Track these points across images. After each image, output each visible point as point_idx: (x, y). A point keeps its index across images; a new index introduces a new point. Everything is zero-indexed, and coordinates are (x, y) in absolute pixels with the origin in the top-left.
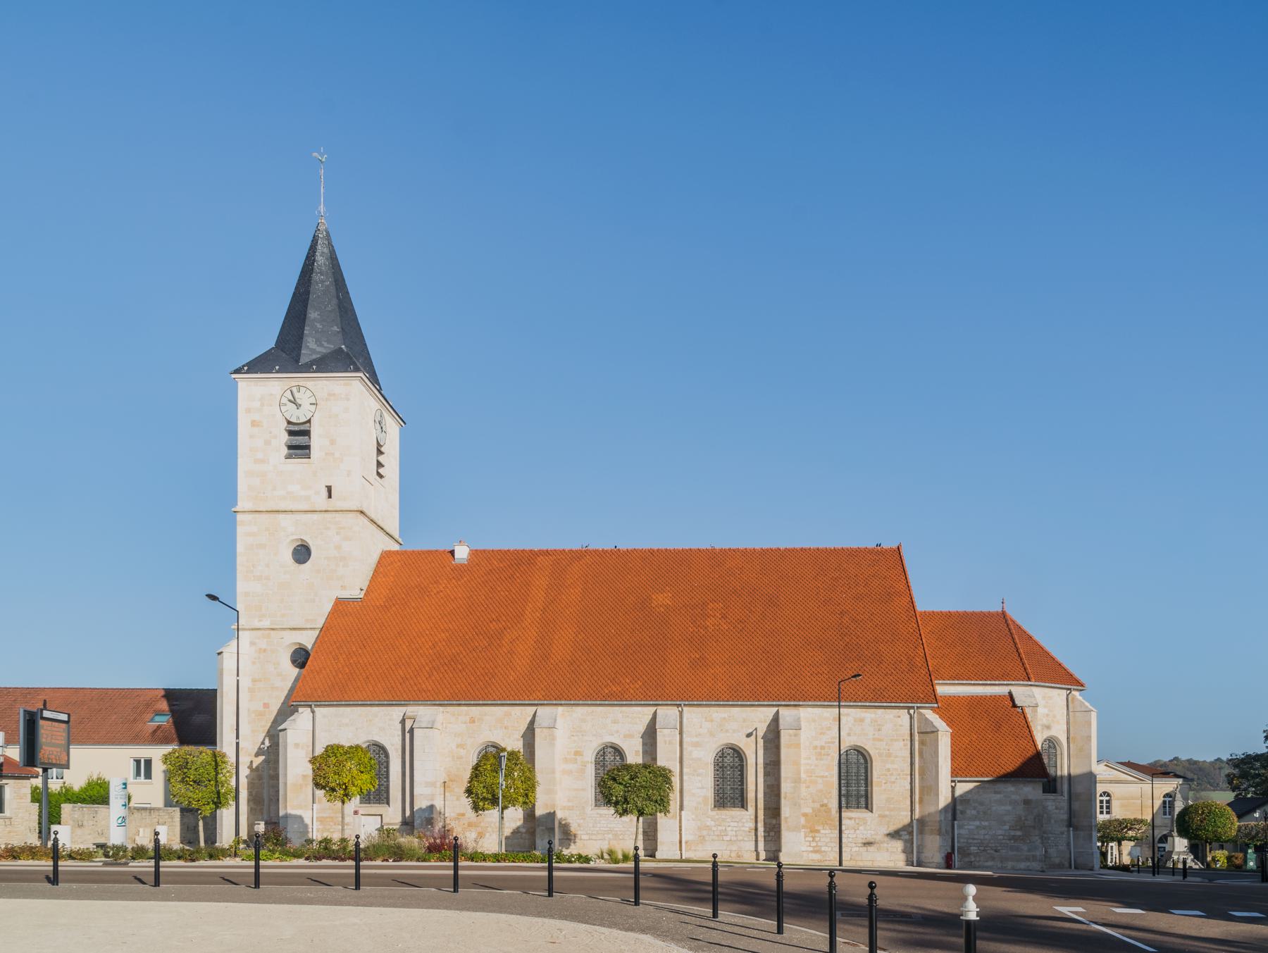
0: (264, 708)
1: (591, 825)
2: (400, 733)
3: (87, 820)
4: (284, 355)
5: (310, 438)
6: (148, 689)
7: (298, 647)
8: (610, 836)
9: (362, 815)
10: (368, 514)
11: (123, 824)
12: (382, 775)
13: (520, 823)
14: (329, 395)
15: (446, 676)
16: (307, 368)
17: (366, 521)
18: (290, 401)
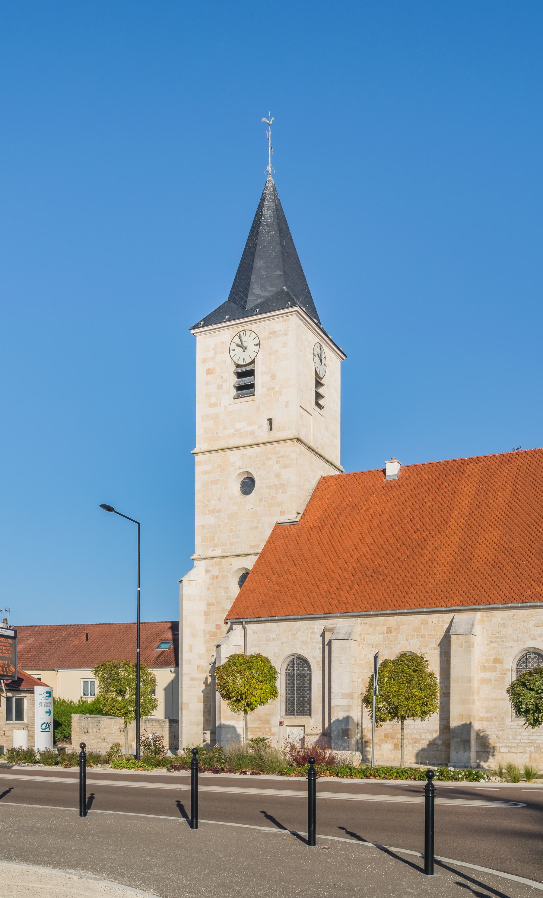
0: (216, 629)
1: (511, 737)
2: (321, 646)
3: (92, 728)
4: (234, 305)
5: (254, 377)
6: (159, 622)
7: (245, 572)
8: (532, 749)
9: (287, 726)
10: (305, 441)
11: (48, 730)
12: (306, 687)
13: (436, 735)
14: (271, 333)
15: (367, 587)
16: (252, 313)
17: (303, 448)
18: (238, 345)
